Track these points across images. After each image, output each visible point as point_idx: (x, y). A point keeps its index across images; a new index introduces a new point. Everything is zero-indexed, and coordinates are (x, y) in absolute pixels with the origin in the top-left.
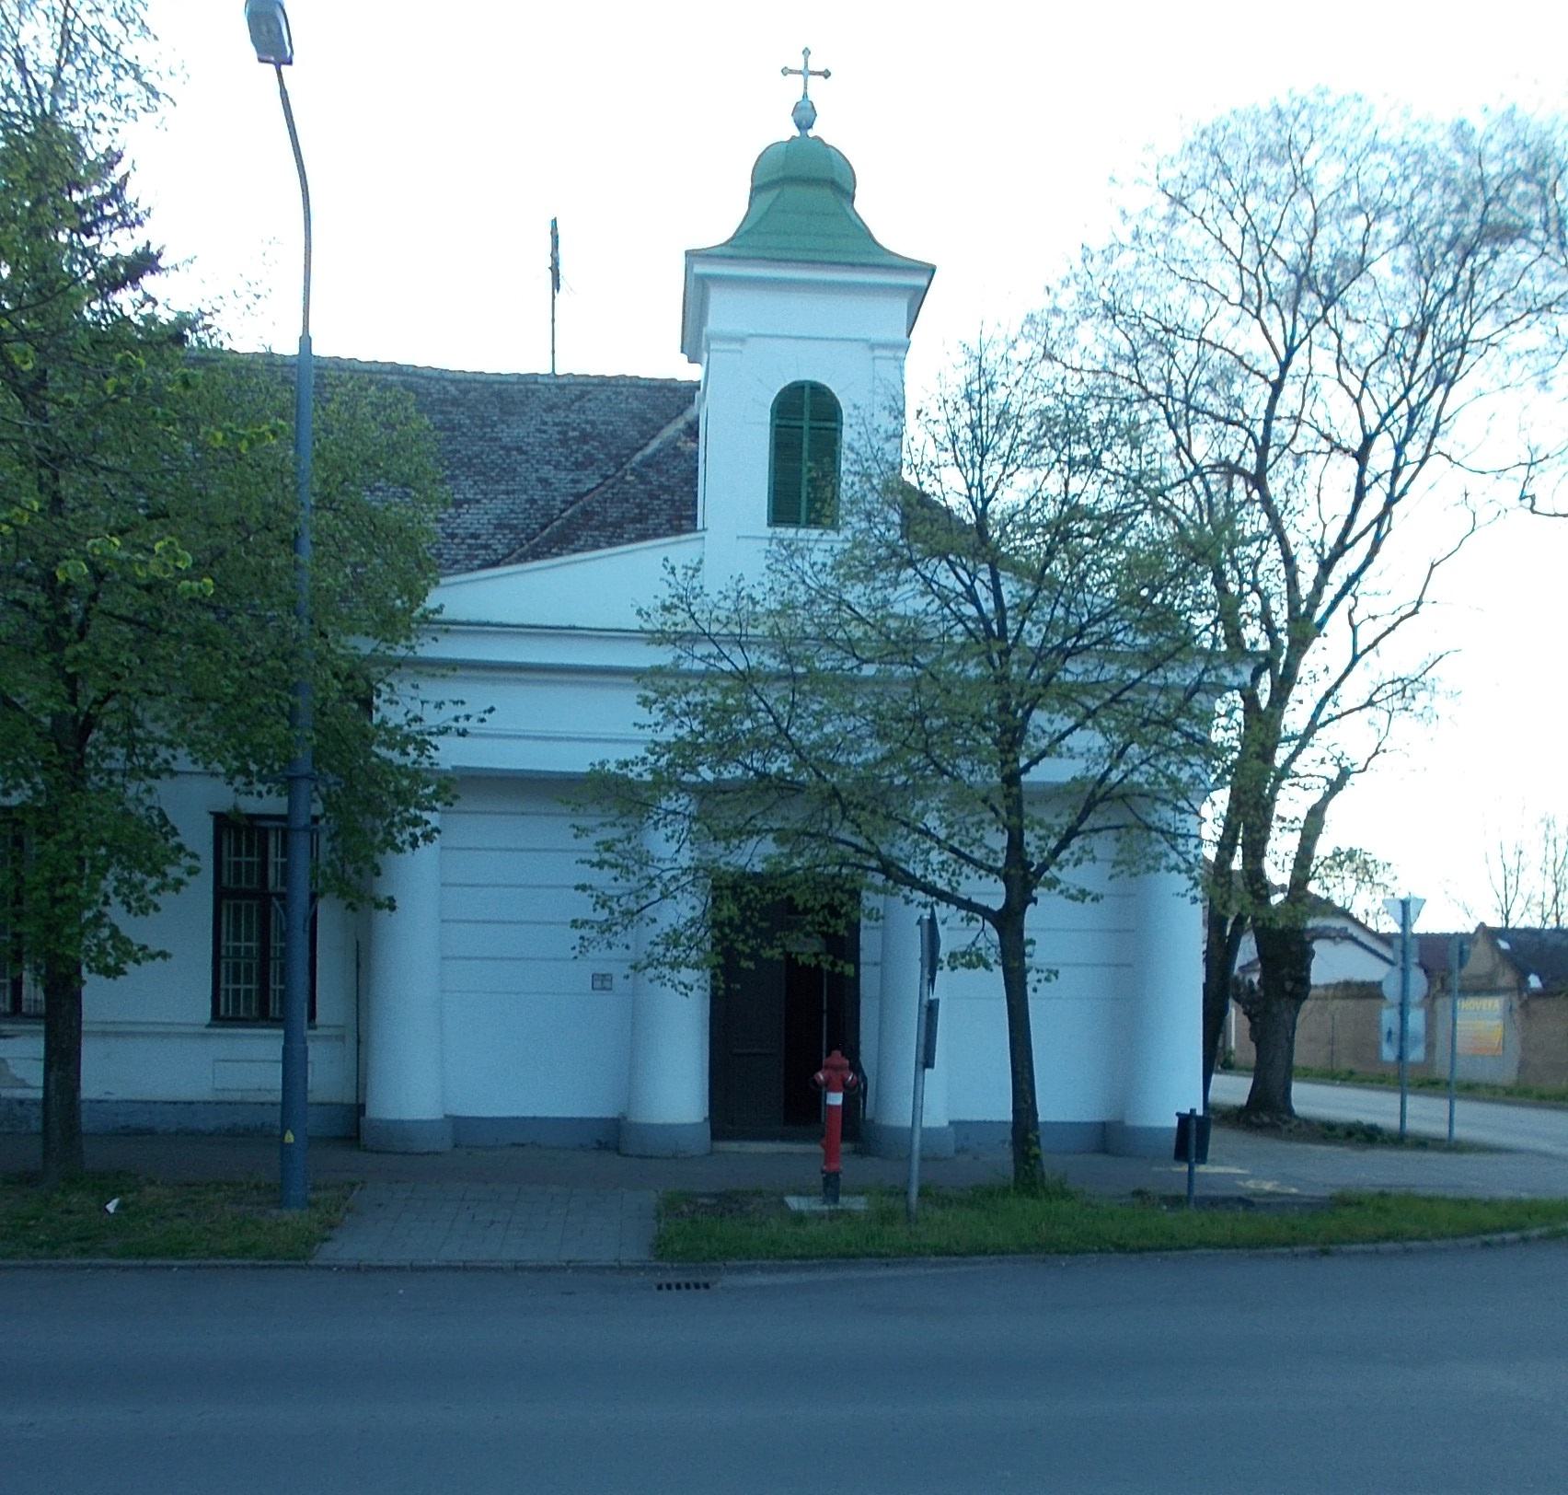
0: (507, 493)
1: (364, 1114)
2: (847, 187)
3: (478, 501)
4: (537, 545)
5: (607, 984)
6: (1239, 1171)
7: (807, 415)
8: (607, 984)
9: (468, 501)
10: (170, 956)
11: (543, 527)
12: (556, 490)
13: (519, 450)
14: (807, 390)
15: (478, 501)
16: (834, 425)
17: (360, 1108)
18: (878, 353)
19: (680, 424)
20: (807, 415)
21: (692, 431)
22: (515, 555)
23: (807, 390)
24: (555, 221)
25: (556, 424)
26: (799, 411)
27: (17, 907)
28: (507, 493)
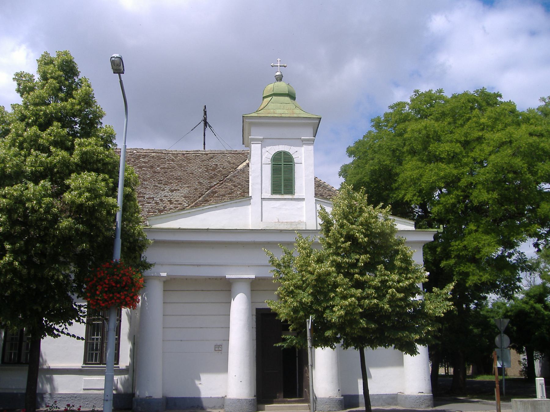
0: (188, 187)
1: (134, 397)
2: (293, 96)
3: (179, 190)
4: (197, 202)
5: (220, 349)
6: (29, 347)
7: (283, 161)
8: (220, 349)
9: (176, 190)
10: (498, 356)
11: (200, 197)
12: (204, 185)
13: (192, 173)
14: (282, 154)
15: (179, 190)
16: (291, 163)
17: (133, 395)
18: (304, 142)
19: (244, 164)
20: (283, 161)
21: (248, 165)
22: (190, 207)
23: (282, 154)
24: (205, 106)
25: (205, 165)
26: (280, 160)
27: (420, 178)
28: (188, 187)
